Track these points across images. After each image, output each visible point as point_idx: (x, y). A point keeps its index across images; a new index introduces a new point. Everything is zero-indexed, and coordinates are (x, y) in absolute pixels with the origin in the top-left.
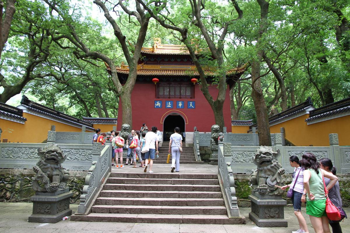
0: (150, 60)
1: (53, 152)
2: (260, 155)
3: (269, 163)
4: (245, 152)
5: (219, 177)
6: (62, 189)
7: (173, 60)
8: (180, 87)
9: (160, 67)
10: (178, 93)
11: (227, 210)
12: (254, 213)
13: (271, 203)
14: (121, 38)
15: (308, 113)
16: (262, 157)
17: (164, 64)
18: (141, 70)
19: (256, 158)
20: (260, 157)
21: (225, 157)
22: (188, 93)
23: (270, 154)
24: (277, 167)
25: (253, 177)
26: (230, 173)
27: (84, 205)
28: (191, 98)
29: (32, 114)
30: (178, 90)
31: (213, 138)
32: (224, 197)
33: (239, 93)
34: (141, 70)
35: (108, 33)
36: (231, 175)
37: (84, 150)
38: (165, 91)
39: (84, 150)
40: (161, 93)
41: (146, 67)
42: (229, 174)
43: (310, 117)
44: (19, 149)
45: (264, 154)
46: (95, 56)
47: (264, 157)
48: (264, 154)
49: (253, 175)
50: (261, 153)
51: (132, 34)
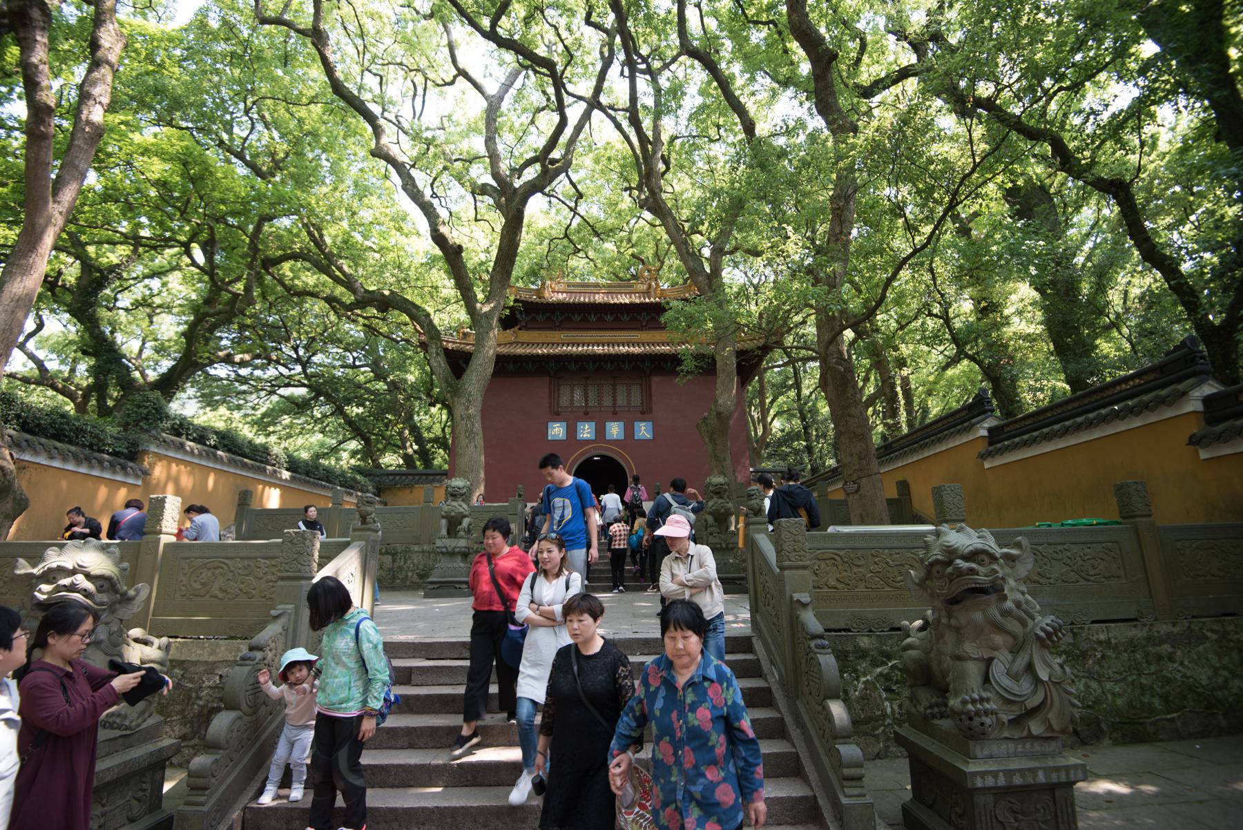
0: (534, 319)
1: (73, 572)
2: (950, 563)
3: (993, 597)
4: (842, 553)
5: (758, 645)
6: (117, 733)
7: (593, 318)
8: (614, 385)
9: (562, 336)
10: (607, 401)
11: (820, 801)
12: (931, 807)
13: (1022, 776)
14: (452, 255)
15: (984, 433)
16: (960, 573)
17: (569, 329)
18: (511, 344)
19: (929, 575)
20: (949, 570)
21: (786, 572)
22: (636, 400)
23: (993, 558)
24: (1026, 612)
25: (910, 652)
26: (814, 637)
27: (202, 804)
28: (642, 413)
29: (250, 475)
30: (607, 389)
31: (711, 513)
32: (794, 732)
33: (762, 403)
34: (511, 344)
35: (421, 246)
36: (823, 647)
37: (273, 562)
38: (573, 395)
39: (273, 562)
40: (564, 400)
41: (525, 336)
42: (813, 644)
43: (990, 444)
44: (246, 562)
45: (966, 558)
46: (385, 303)
47: (972, 570)
48: (966, 558)
49: (910, 647)
50: (951, 553)
51: (479, 240)
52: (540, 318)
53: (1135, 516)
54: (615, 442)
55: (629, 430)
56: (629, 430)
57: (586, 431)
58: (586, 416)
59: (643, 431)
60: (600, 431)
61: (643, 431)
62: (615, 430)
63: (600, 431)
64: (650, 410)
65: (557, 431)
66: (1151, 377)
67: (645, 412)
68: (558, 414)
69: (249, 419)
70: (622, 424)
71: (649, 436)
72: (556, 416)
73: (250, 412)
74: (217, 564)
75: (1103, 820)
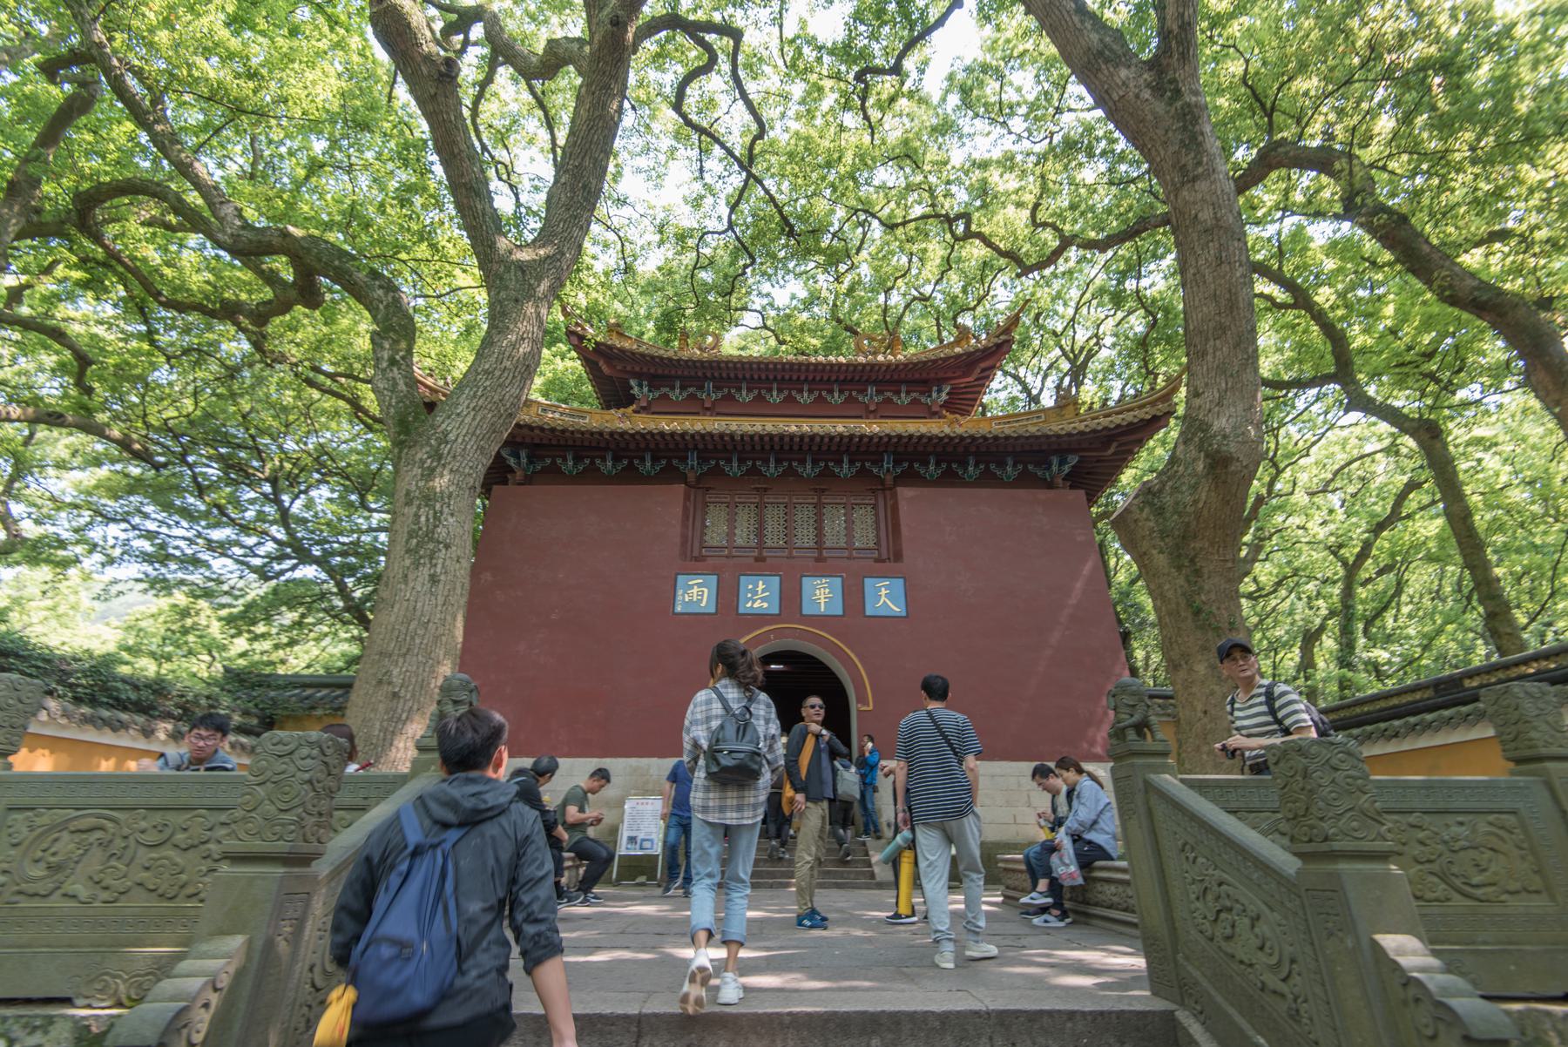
10: (805, 537)
22: (865, 535)
52: (676, 395)
53: (1334, 856)
54: (822, 620)
55: (853, 596)
56: (853, 596)
57: (759, 595)
58: (760, 564)
59: (885, 597)
60: (791, 597)
61: (885, 597)
62: (822, 595)
63: (791, 597)
64: (898, 556)
65: (696, 594)
66: (1429, 693)
67: (889, 557)
68: (700, 559)
69: (224, 612)
70: (838, 581)
71: (897, 609)
72: (695, 558)
73: (225, 600)
74: (92, 821)
75: (869, 940)
